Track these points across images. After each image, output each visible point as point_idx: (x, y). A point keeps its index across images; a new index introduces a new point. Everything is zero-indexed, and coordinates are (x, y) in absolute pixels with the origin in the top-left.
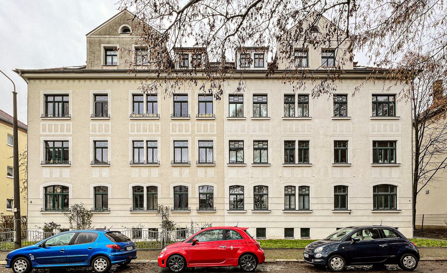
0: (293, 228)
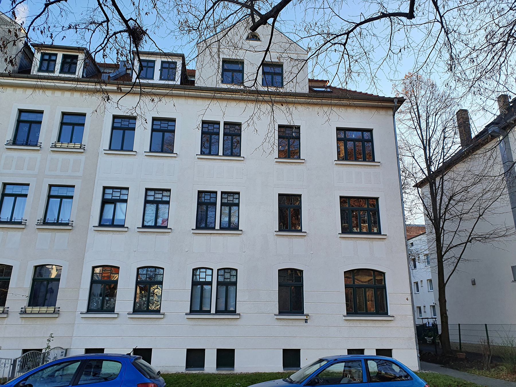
0: (204, 349)
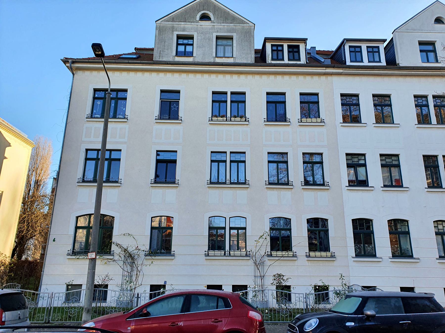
0: (82, 285)
